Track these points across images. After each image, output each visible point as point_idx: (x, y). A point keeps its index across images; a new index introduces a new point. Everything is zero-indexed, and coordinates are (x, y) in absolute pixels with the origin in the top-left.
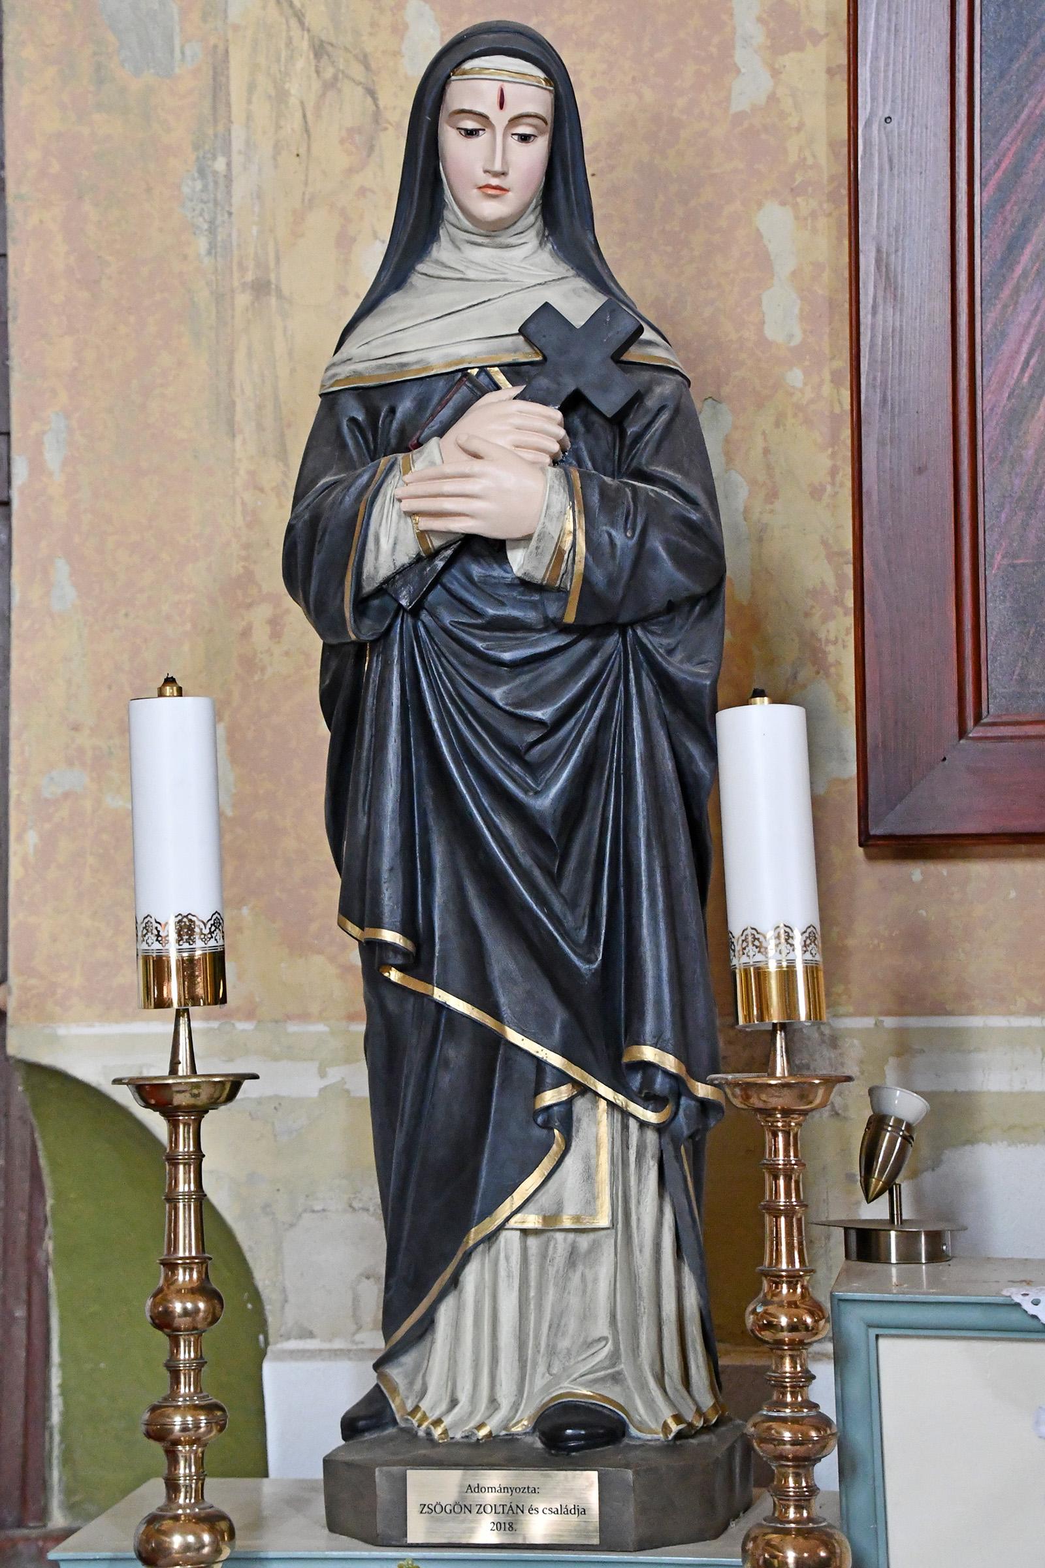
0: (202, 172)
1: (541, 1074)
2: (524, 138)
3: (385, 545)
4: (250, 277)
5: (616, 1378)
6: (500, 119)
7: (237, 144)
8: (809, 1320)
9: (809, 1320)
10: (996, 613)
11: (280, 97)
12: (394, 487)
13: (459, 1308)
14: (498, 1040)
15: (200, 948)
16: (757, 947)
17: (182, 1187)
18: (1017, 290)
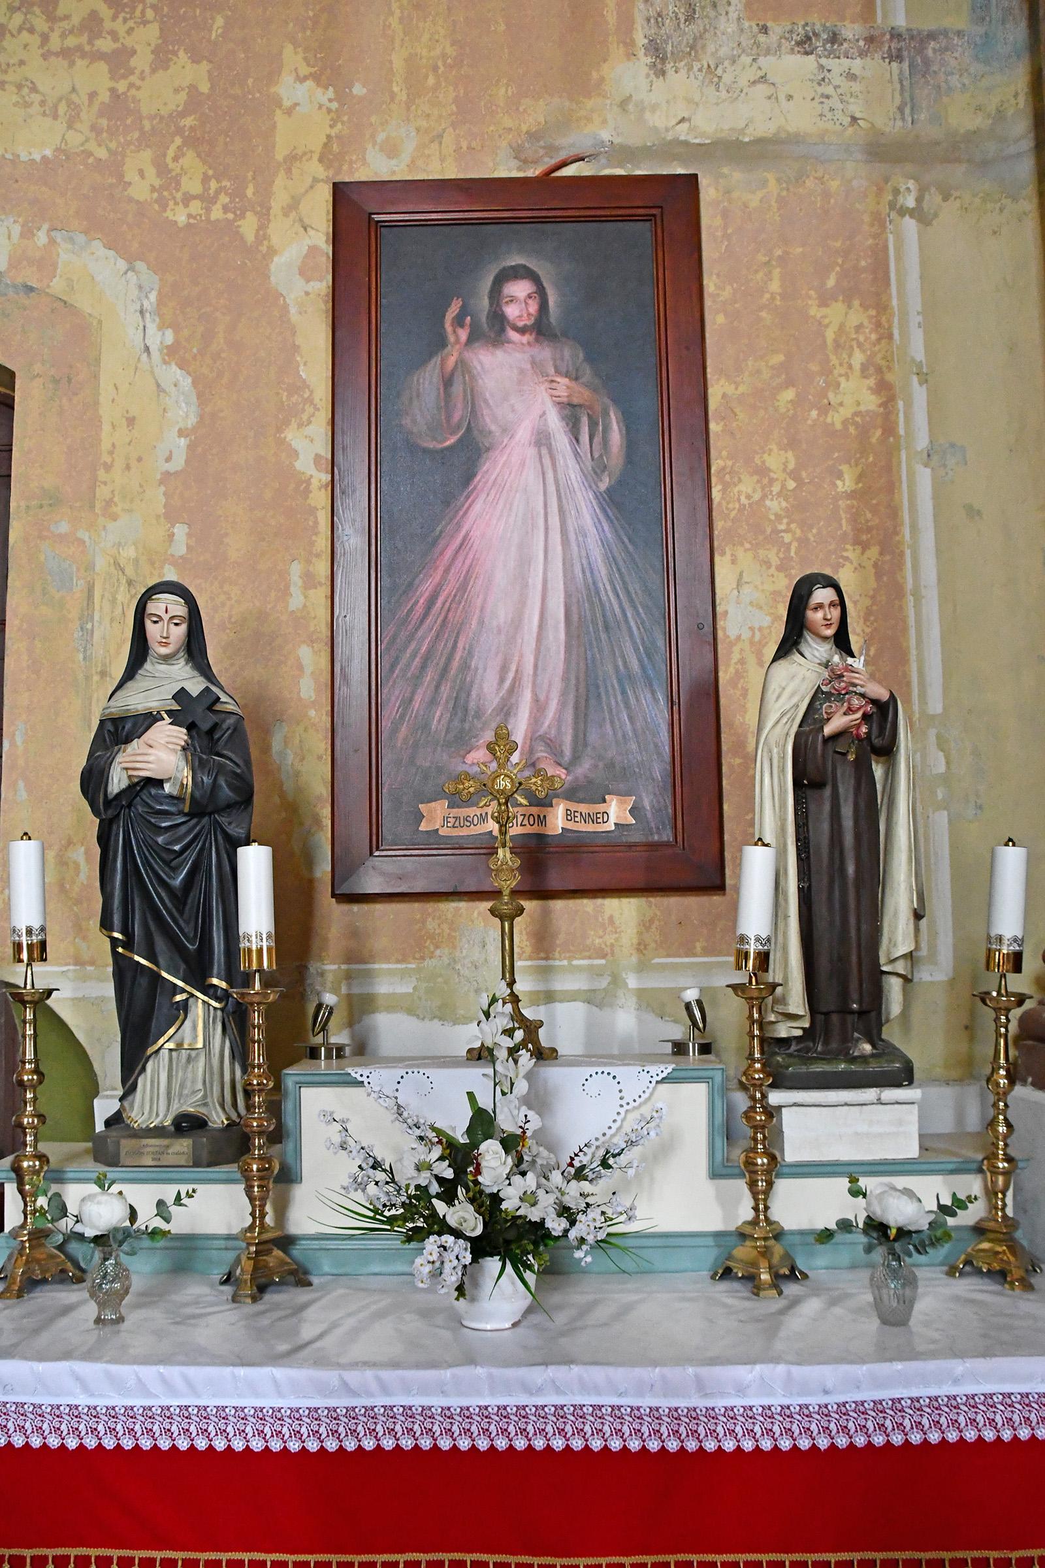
0: (82, 629)
1: (175, 989)
2: (176, 624)
3: (116, 780)
4: (99, 669)
5: (206, 1105)
6: (166, 617)
7: (96, 617)
8: (265, 1082)
9: (265, 1082)
10: (386, 806)
11: (113, 601)
12: (119, 758)
13: (146, 1078)
14: (160, 976)
15: (35, 939)
17: (28, 1032)
18: (394, 682)
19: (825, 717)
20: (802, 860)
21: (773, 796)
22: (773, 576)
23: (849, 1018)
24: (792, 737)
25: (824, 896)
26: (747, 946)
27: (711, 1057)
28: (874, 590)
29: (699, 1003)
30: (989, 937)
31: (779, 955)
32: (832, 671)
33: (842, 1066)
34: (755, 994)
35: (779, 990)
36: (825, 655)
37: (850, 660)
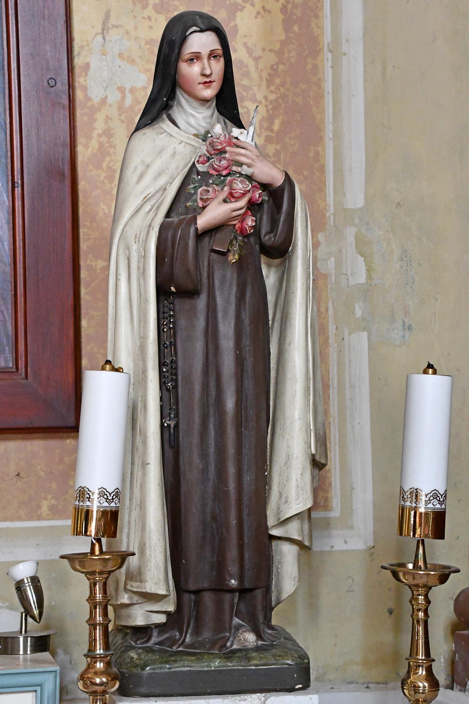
16: (438, 501)
19: (200, 204)
20: (168, 390)
21: (131, 306)
22: (150, 18)
23: (227, 597)
24: (157, 229)
25: (196, 439)
26: (88, 503)
27: (46, 655)
28: (282, 42)
29: (35, 580)
30: (402, 491)
31: (135, 514)
32: (212, 144)
33: (216, 664)
34: (98, 568)
35: (133, 561)
36: (204, 125)
37: (236, 132)
